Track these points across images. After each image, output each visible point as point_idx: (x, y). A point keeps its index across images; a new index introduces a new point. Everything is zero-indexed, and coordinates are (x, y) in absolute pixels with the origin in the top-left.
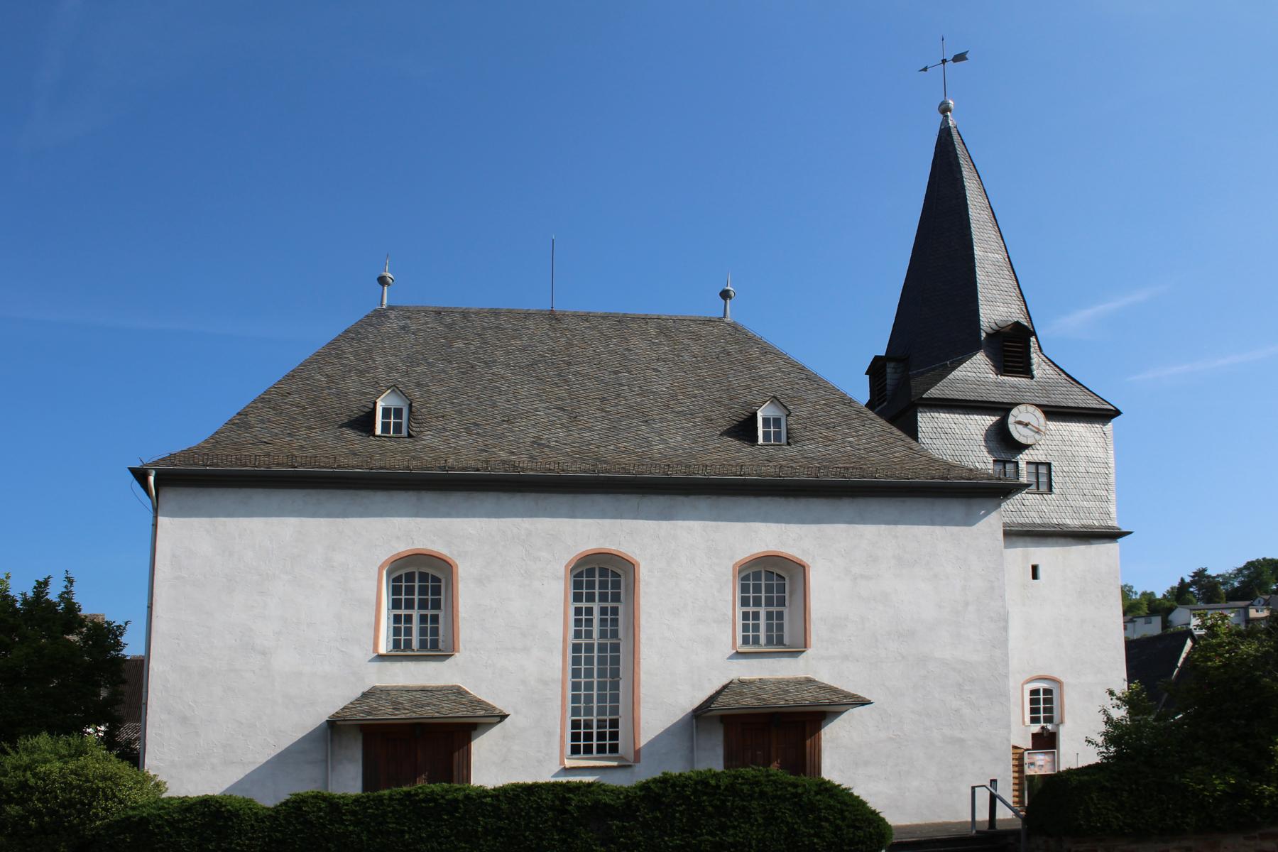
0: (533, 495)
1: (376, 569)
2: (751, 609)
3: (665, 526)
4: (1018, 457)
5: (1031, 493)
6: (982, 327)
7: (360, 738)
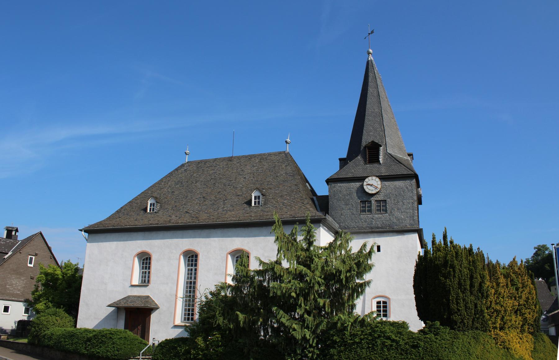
0: (173, 231)
1: (133, 257)
2: (144, 270)
3: (207, 240)
4: (371, 199)
5: (377, 214)
6: (362, 145)
7: (125, 312)
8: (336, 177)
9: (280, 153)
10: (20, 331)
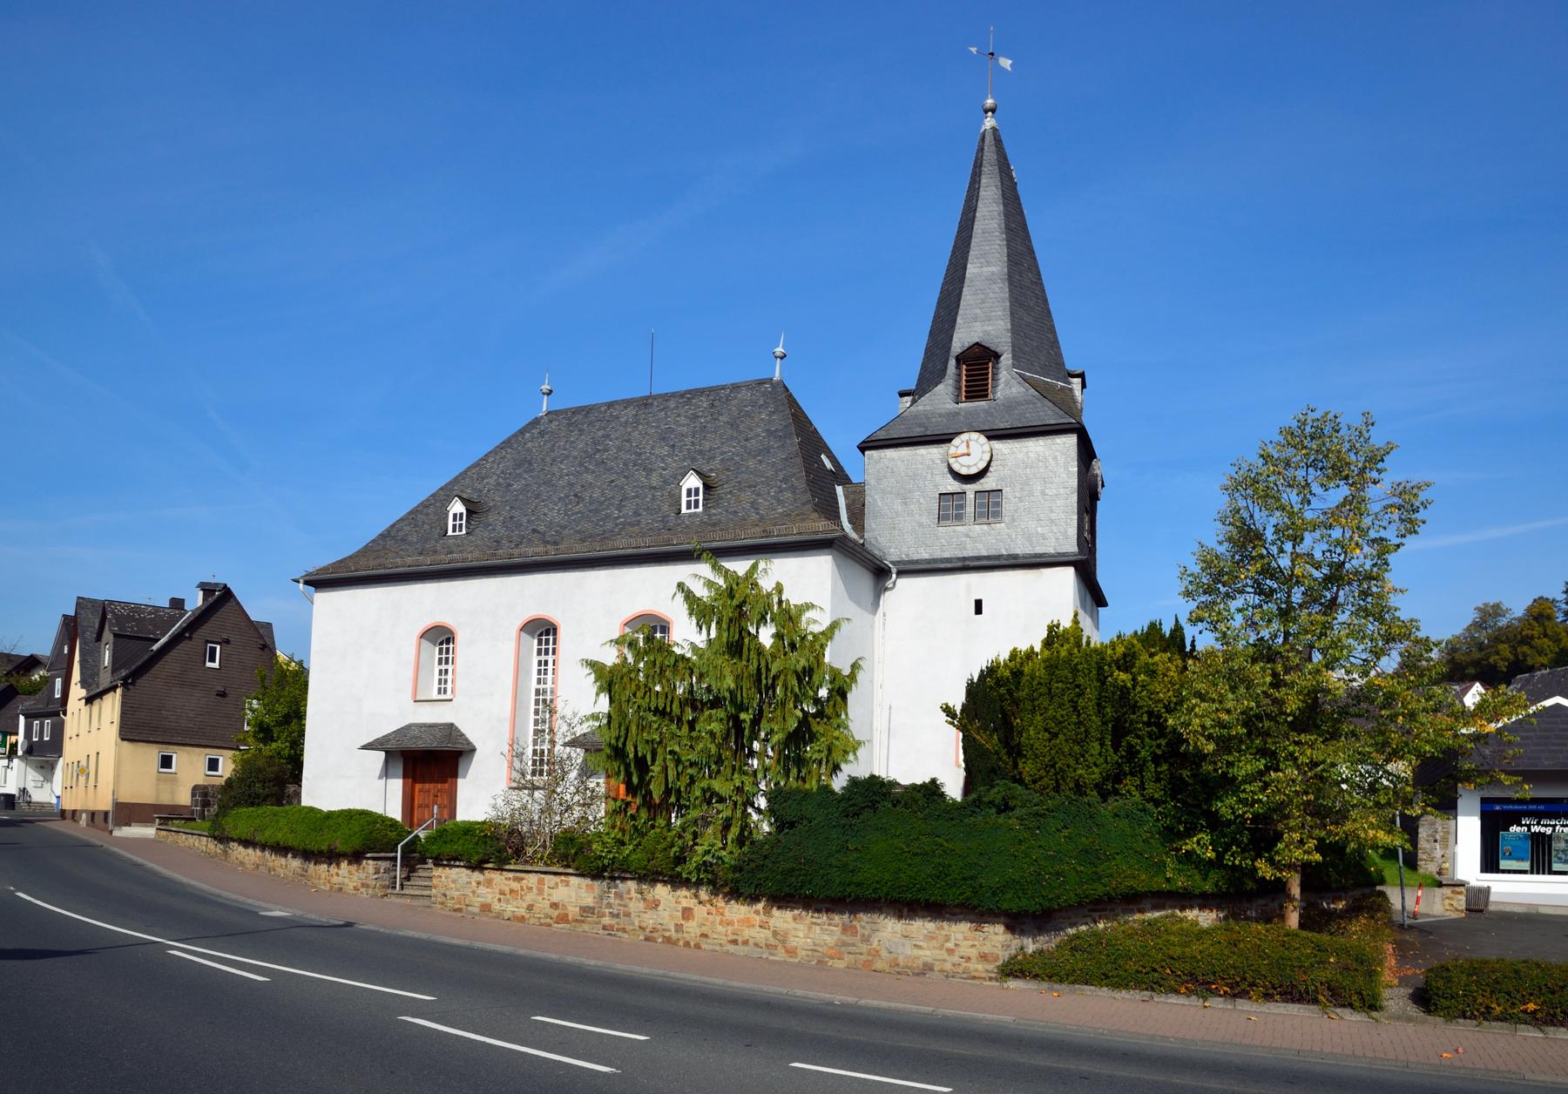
8: (882, 435)
9: (761, 383)
10: (198, 808)
